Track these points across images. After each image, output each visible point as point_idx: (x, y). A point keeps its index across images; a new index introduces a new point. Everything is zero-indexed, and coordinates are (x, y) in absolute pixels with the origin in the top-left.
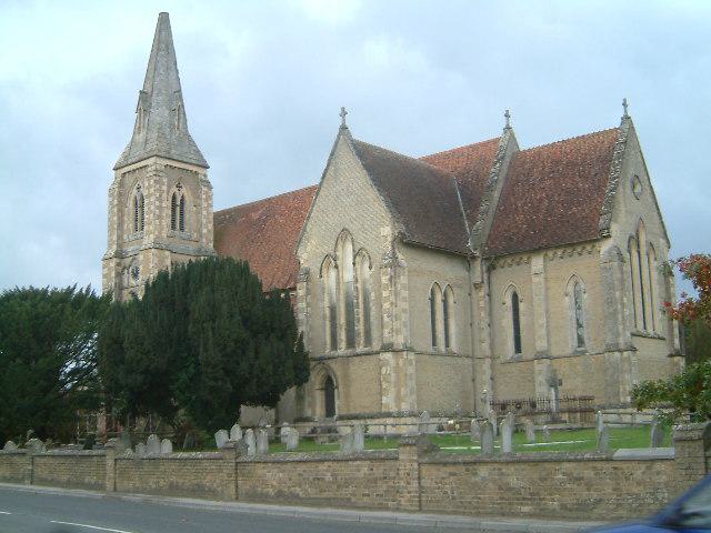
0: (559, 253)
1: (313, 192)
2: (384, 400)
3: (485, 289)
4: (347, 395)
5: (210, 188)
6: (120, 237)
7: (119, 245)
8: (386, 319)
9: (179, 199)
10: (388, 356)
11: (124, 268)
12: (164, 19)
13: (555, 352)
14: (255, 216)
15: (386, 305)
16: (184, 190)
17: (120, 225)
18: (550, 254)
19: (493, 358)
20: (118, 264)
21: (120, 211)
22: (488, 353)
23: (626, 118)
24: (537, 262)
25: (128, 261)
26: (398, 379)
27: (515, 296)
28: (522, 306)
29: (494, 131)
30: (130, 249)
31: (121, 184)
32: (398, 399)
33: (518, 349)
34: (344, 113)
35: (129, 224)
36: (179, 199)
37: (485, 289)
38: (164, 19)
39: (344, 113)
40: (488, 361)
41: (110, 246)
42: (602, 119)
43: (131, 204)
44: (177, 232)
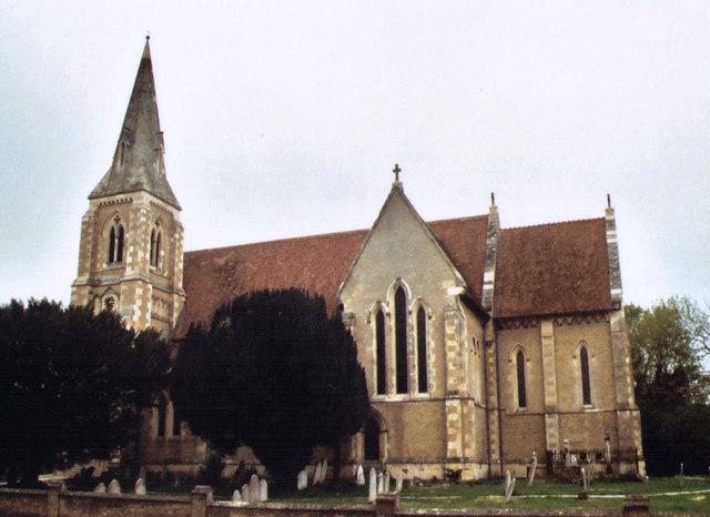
0: (569, 320)
1: (361, 236)
2: (451, 445)
3: (493, 347)
4: (400, 437)
5: (182, 229)
6: (93, 265)
7: (93, 274)
8: (451, 367)
9: (156, 236)
10: (456, 403)
11: (96, 296)
12: (146, 65)
13: (563, 407)
14: (221, 261)
15: (451, 355)
16: (161, 227)
17: (95, 253)
18: (560, 320)
19: (500, 410)
20: (91, 293)
21: (95, 240)
22: (496, 405)
23: (494, 208)
24: (547, 328)
25: (101, 290)
26: (463, 426)
27: (520, 356)
28: (528, 365)
29: (481, 209)
30: (106, 279)
31: (97, 213)
32: (465, 446)
33: (522, 402)
34: (397, 170)
35: (104, 254)
36: (156, 236)
37: (493, 347)
38: (146, 65)
39: (397, 170)
40: (496, 412)
41: (81, 273)
42: (596, 211)
43: (106, 234)
44: (114, 266)
